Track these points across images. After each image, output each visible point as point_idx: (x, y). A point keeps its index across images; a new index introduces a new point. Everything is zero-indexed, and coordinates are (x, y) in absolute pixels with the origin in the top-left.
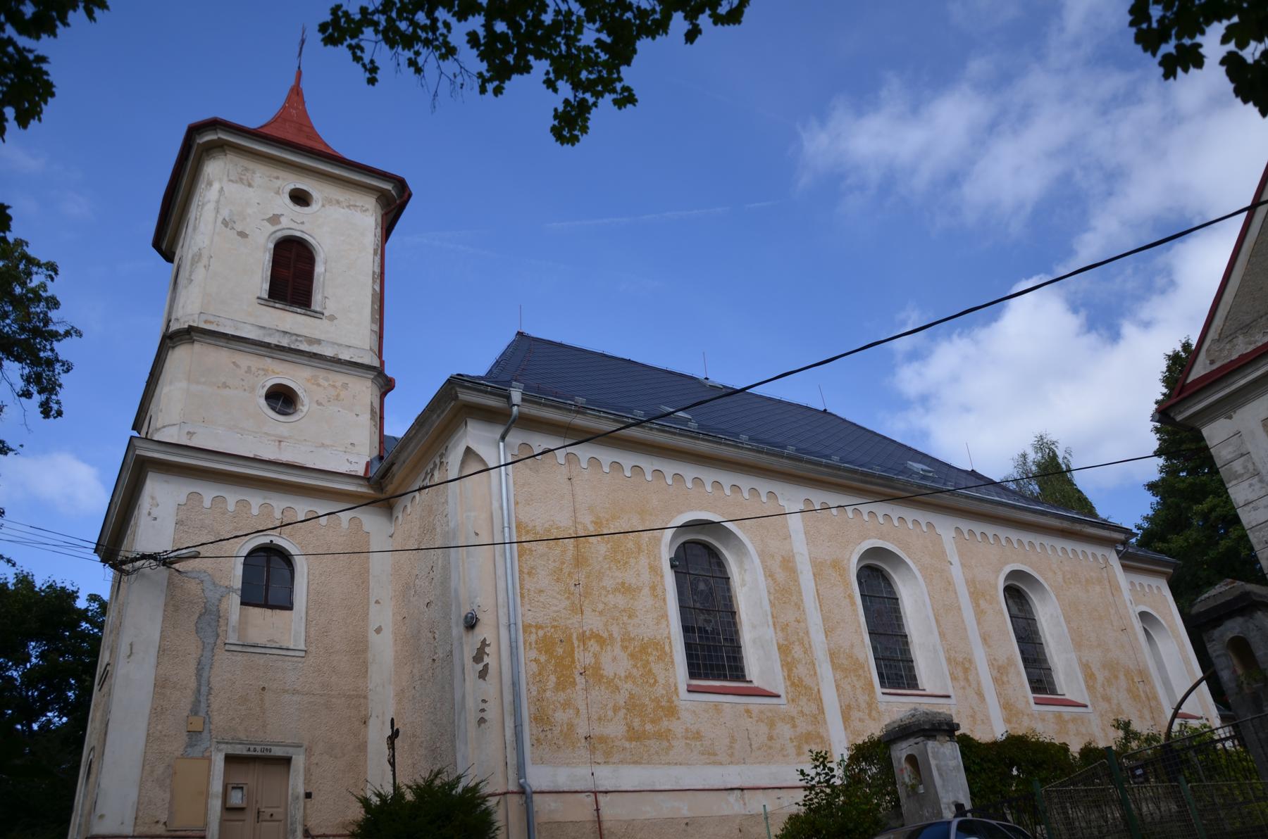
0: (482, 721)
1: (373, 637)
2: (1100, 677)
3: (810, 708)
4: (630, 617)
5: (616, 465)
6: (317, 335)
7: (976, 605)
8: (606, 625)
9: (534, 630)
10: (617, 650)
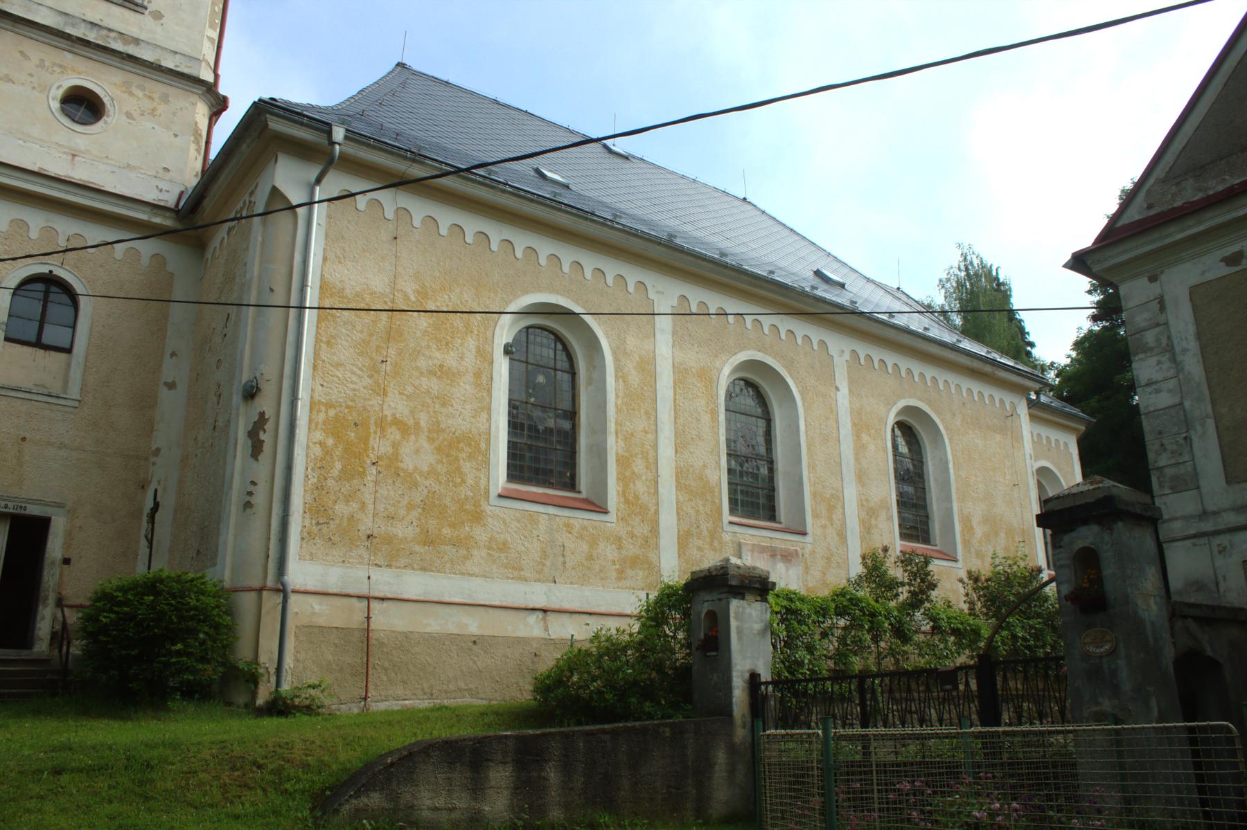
0: (248, 505)
1: (164, 393)
2: (979, 531)
3: (642, 530)
4: (443, 405)
5: (403, 212)
6: (134, 32)
7: (858, 437)
8: (412, 412)
9: (323, 409)
10: (424, 443)
